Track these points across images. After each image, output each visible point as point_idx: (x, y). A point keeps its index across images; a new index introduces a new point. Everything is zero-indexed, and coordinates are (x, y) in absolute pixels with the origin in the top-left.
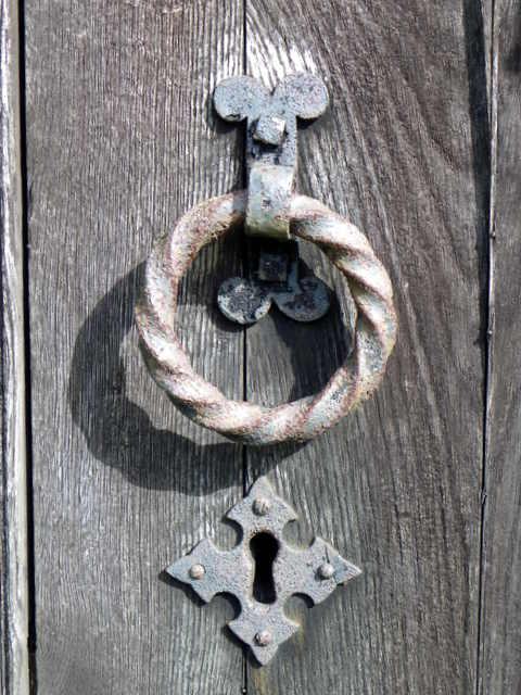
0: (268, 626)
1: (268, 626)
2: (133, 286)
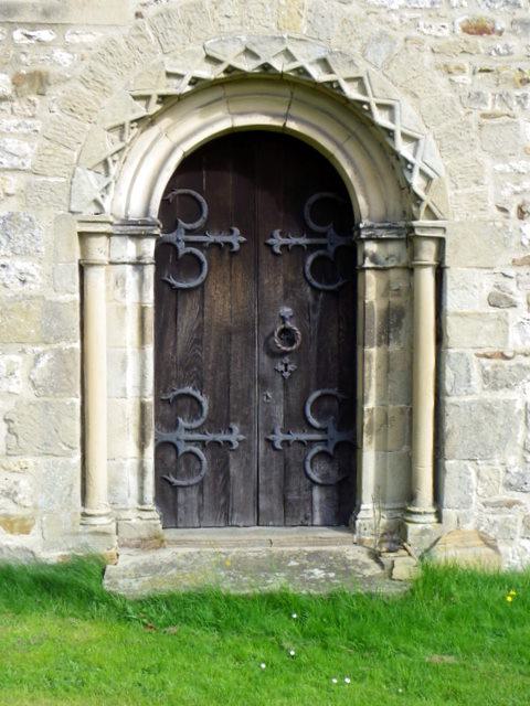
0: (287, 374)
1: (287, 374)
2: (273, 334)
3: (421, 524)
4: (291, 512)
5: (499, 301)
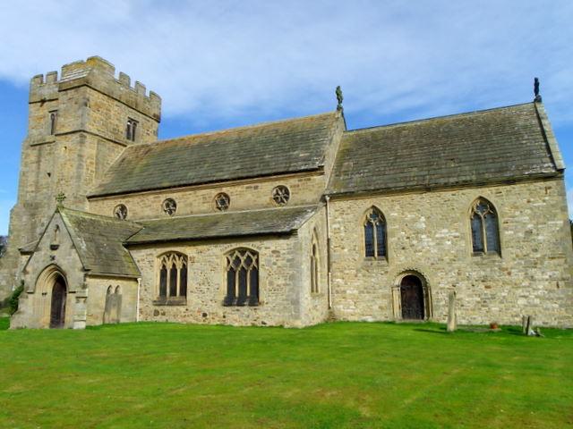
3: (431, 318)
4: (418, 318)
5: (437, 293)
